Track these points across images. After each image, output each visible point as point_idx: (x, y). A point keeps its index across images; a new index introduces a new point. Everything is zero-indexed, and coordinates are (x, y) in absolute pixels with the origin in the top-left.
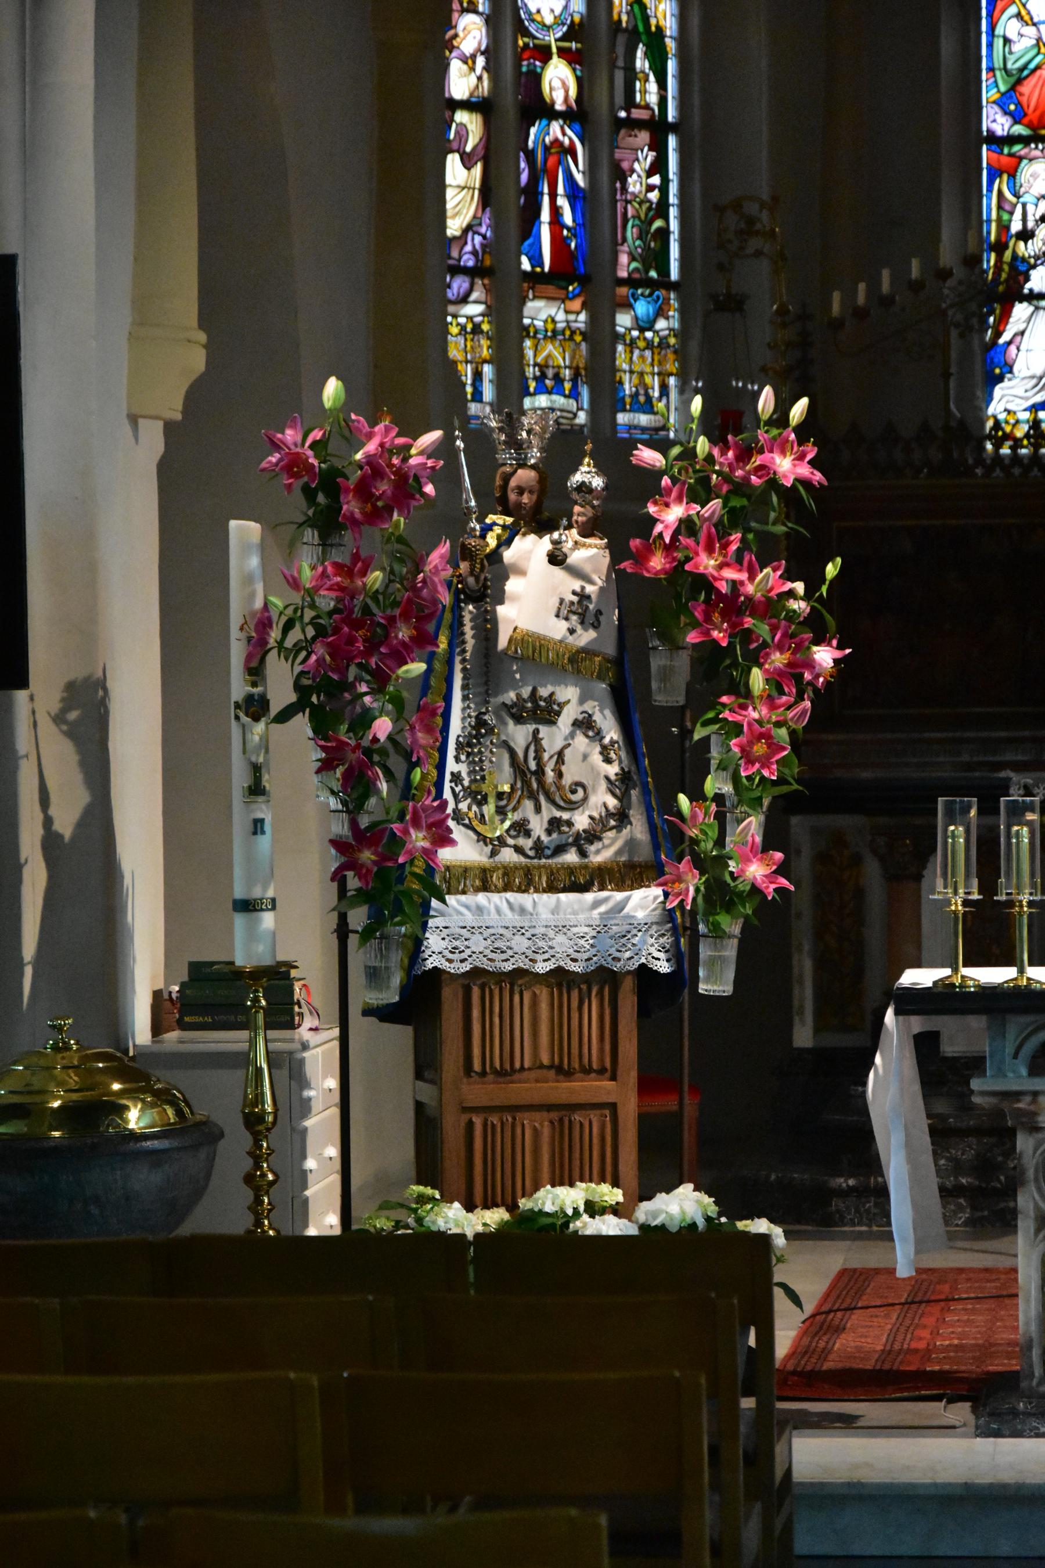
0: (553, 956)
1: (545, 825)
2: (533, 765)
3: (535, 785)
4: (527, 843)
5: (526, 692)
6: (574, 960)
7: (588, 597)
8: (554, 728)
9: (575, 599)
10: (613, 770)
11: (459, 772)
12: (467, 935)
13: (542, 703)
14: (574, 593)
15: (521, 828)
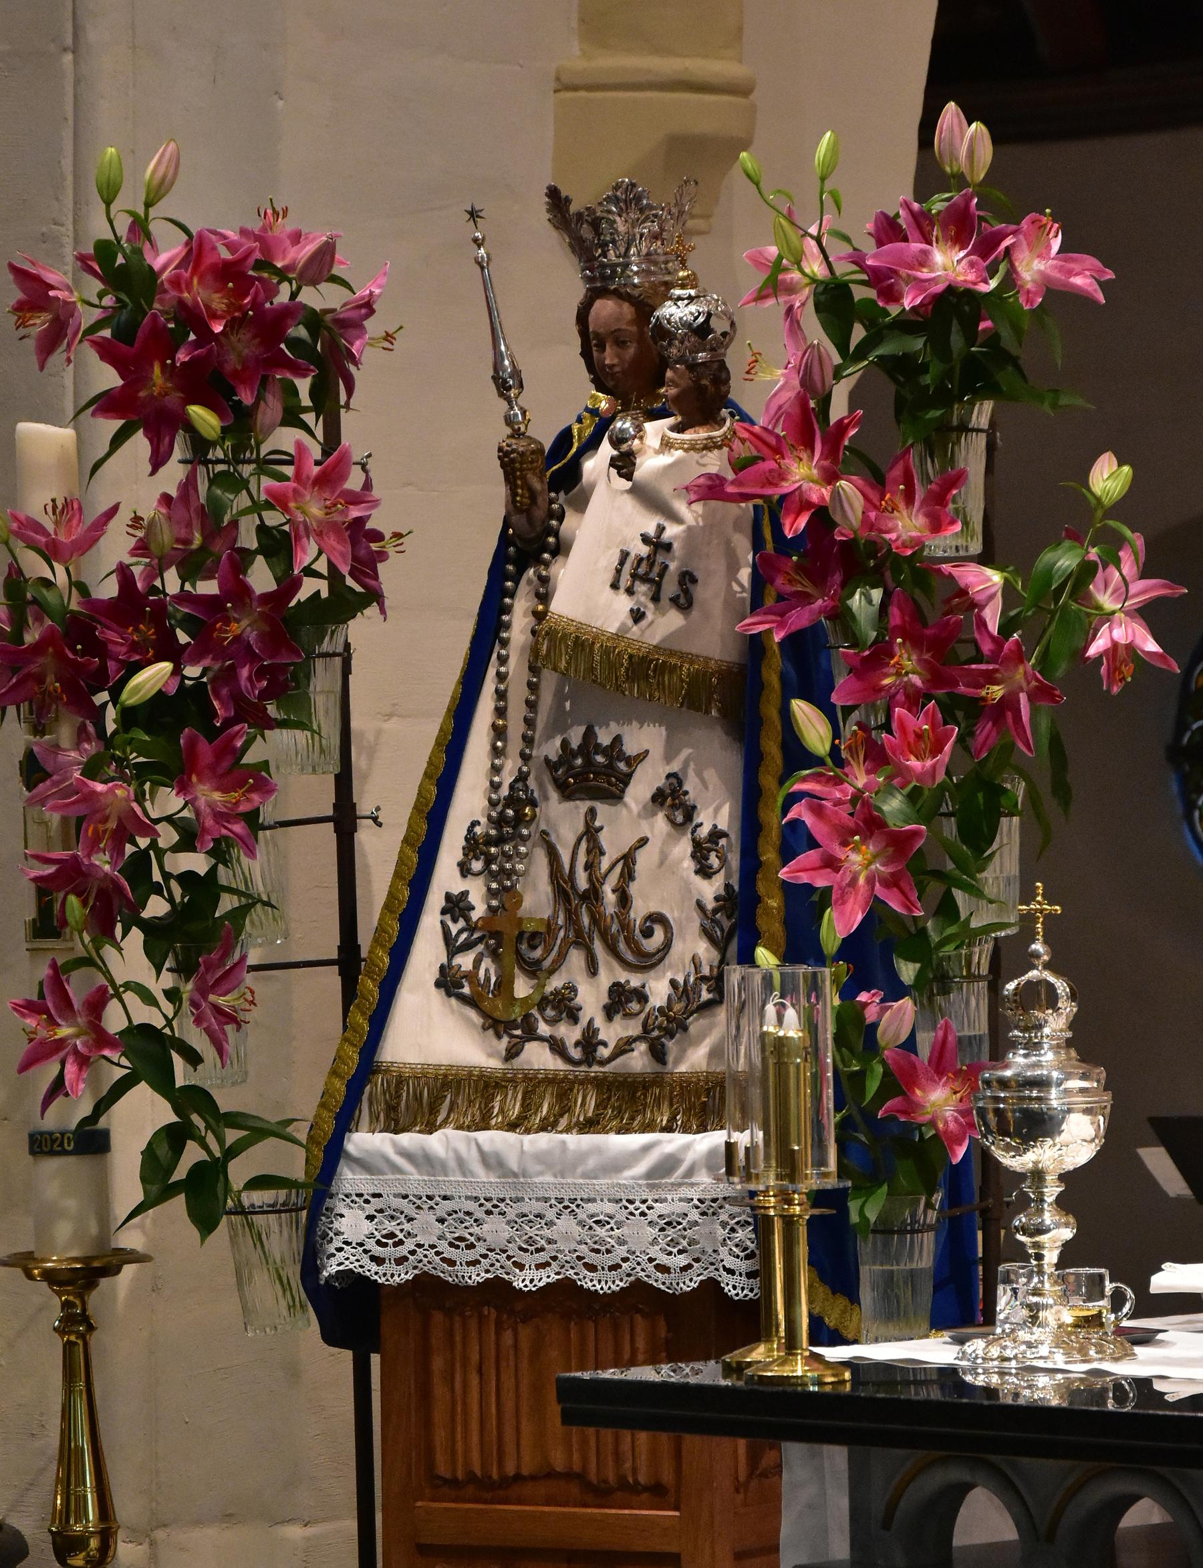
0: (555, 1258)
1: (605, 999)
2: (582, 883)
3: (586, 920)
4: (570, 1034)
5: (576, 737)
6: (592, 1268)
7: (668, 547)
8: (619, 807)
9: (644, 550)
10: (709, 890)
11: (465, 894)
12: (410, 1210)
13: (600, 759)
14: (645, 539)
15: (564, 1005)
